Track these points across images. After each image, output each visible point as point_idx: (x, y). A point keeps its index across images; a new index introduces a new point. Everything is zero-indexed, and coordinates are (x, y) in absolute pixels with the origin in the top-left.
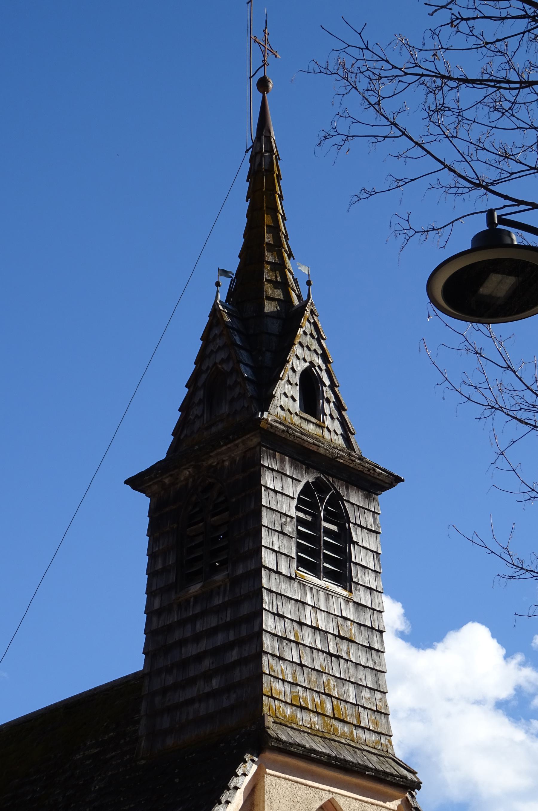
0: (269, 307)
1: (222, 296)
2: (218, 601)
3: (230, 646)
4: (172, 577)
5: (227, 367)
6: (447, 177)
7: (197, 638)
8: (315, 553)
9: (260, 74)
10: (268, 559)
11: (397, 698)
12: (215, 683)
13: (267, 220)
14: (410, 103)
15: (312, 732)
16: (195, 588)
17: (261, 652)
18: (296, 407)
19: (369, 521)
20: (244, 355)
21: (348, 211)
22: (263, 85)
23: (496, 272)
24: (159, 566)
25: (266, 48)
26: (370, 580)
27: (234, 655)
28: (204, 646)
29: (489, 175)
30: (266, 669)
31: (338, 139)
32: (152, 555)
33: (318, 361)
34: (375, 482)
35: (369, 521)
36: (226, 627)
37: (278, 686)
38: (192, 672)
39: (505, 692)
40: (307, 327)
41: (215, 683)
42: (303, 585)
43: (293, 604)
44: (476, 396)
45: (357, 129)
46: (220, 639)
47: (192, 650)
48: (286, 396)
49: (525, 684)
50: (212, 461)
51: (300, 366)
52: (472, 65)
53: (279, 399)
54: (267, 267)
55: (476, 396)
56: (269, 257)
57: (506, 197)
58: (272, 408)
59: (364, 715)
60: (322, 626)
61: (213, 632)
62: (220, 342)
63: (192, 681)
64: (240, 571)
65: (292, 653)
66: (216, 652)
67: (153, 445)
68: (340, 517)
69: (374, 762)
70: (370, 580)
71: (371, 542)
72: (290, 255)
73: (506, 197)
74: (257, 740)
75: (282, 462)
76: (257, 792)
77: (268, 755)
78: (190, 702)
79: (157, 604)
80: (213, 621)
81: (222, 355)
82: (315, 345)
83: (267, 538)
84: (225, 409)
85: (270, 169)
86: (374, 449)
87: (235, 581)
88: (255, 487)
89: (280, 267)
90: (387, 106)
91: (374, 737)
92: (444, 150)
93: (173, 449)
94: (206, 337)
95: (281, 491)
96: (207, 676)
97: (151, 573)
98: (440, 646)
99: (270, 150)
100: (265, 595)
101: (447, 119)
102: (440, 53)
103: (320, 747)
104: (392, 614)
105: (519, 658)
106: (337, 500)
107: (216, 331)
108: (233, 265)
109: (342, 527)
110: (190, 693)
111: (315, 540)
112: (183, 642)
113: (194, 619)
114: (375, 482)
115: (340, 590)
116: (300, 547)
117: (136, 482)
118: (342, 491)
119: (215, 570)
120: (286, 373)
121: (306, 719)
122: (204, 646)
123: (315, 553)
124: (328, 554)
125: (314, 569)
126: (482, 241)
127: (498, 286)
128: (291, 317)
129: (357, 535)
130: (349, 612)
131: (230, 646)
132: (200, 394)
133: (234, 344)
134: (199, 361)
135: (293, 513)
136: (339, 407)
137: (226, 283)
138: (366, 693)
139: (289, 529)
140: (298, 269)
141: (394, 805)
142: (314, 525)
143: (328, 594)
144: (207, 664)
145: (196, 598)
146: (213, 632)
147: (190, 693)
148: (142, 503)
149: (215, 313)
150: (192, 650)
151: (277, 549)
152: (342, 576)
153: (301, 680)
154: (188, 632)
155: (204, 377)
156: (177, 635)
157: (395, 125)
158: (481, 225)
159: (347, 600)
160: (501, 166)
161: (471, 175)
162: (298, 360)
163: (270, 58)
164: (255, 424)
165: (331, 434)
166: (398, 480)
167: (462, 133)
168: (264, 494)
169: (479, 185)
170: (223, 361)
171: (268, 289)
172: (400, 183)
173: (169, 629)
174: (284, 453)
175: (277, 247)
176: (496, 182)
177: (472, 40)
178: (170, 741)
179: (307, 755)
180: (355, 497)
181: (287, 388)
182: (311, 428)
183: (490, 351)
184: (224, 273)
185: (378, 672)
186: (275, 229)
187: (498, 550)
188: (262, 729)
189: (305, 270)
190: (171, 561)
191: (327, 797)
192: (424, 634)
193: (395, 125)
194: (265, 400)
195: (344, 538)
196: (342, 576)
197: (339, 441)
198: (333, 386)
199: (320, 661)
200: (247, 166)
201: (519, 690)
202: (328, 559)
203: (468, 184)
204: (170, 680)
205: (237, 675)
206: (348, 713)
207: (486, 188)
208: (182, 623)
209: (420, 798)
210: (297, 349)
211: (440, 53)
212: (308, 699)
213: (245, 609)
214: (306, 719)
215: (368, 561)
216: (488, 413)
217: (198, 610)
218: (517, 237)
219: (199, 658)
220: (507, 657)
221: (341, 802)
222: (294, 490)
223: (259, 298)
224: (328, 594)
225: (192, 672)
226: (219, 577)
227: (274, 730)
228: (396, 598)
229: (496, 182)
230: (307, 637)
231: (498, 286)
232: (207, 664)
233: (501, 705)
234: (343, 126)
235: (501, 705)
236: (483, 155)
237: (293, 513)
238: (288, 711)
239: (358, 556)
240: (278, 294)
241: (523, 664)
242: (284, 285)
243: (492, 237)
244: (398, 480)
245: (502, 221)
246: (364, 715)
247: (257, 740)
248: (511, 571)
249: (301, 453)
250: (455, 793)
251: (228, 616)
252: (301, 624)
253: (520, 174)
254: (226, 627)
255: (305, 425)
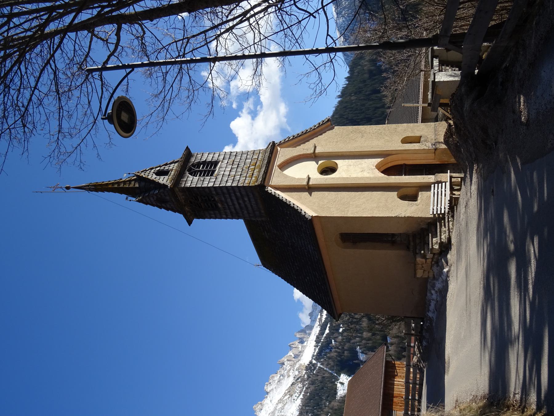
0: (137, 185)
1: (134, 199)
2: (223, 199)
3: (236, 195)
4: (217, 212)
5: (155, 197)
6: (93, 132)
7: (234, 205)
8: (209, 171)
9: (65, 189)
10: (211, 185)
11: (251, 148)
12: (246, 199)
13: (110, 186)
14: (68, 144)
15: (259, 172)
16: (220, 205)
17: (237, 186)
18: (166, 177)
19: (199, 156)
20: (152, 192)
21: (315, 147)
22: (68, 188)
23: (120, 117)
24: (213, 216)
25: (56, 187)
26: (216, 156)
27: (238, 194)
28: (236, 203)
29: (92, 120)
30: (242, 185)
31: (82, 165)
32: (210, 218)
33: (153, 171)
34: (188, 154)
35: (199, 156)
36: (230, 197)
37: (246, 181)
38: (243, 206)
39: (249, 117)
40: (142, 174)
41: (246, 199)
42: (218, 175)
43: (224, 177)
44: (160, 124)
45: (78, 159)
46: (234, 198)
47: (237, 206)
48: (163, 180)
49: (248, 111)
50: (183, 201)
51: (154, 176)
52: (54, 124)
53: (164, 182)
54: (125, 186)
55: (160, 124)
56: (122, 185)
57: (98, 114)
58: (167, 184)
59: (254, 157)
60: (229, 169)
61: (232, 200)
62: (148, 200)
63: (246, 206)
64: (214, 192)
65: (238, 177)
66: (237, 199)
67: (179, 218)
68: (199, 164)
69: (267, 154)
70: (216, 156)
71: (206, 155)
72: (121, 179)
73: (98, 114)
74: (262, 187)
75: (183, 181)
76: (277, 187)
77: (266, 184)
78: (251, 206)
79: (224, 216)
80: (229, 200)
81: (152, 199)
82: (148, 172)
83: (205, 185)
84: (168, 198)
85: (95, 185)
86: (179, 155)
87: (217, 194)
88: (190, 189)
89: (125, 182)
90: (70, 149)
91: (260, 154)
92: (84, 133)
93: (180, 213)
94: (147, 204)
95: (191, 181)
96: (244, 201)
97: (216, 218)
98: (237, 136)
99: (89, 185)
100: (221, 185)
101: (74, 132)
102: (52, 133)
103: (263, 169)
104: (228, 149)
105: (240, 113)
106: (193, 165)
107: (144, 201)
108: (124, 196)
109: (201, 164)
110: (249, 206)
111: (205, 171)
112: (235, 209)
113: (228, 205)
114: (188, 154)
115: (219, 164)
116: (204, 175)
117: (190, 223)
118: (191, 164)
119: (214, 200)
120: (157, 180)
121: (256, 174)
122: (236, 203)
123: (209, 171)
124: (209, 168)
125: (213, 172)
126: (111, 121)
127: (125, 117)
128: (140, 179)
129: (204, 159)
130: (226, 161)
131: (236, 195)
132: (163, 205)
133: (148, 195)
134: (153, 205)
135: (198, 177)
136: (166, 164)
137: (130, 198)
138: (248, 157)
139: (202, 179)
140: (125, 177)
141: (279, 149)
142: (201, 172)
143: (220, 167)
144: (241, 202)
145: (222, 205)
146: (232, 200)
147: (249, 206)
148: (195, 221)
149: (139, 201)
150: (237, 206)
151: (208, 182)
152: (216, 163)
153: (245, 175)
154: (232, 207)
155: (158, 204)
156: (233, 210)
157: (76, 148)
158: (106, 122)
159: (222, 162)
160: (88, 116)
161: (92, 125)
162: (152, 176)
163: (59, 186)
164: (172, 189)
165: (174, 167)
166: (187, 147)
167: (78, 127)
168: (192, 186)
169: (95, 122)
170: (153, 199)
171: (131, 186)
172: (95, 146)
173: (231, 212)
174: (180, 181)
175: (118, 183)
176: (94, 117)
177: (46, 123)
178: (263, 212)
179: (266, 173)
180: (193, 160)
181: (161, 180)
182: (173, 173)
183: (146, 120)
184: (127, 199)
185: (242, 153)
186: (113, 184)
187: (206, 118)
188: (258, 186)
189: (125, 175)
190: (212, 212)
191: (277, 167)
192: (234, 140)
193: (76, 148)
194: (165, 186)
195: (204, 163)
196: (216, 163)
197: (176, 164)
198: (160, 166)
199: (240, 170)
200: (94, 192)
201: (249, 113)
202: (211, 168)
203: (95, 126)
204: (246, 212)
205: (244, 193)
206: (254, 162)
207: (96, 120)
208: (229, 209)
209: (277, 141)
210: (149, 177)
211: (52, 133)
212: (250, 173)
213: (225, 191)
214: (256, 174)
215: (211, 156)
216: (165, 121)
217: (226, 204)
218: (109, 111)
219: (239, 204)
220: (240, 117)
221: (278, 163)
222: (191, 177)
223: (134, 188)
224: (220, 167)
225: (243, 206)
226: (216, 199)
227: (259, 182)
228: (223, 148)
229: (94, 117)
230: (233, 173)
231: (125, 117)
232: (241, 202)
233: (253, 118)
234: (77, 163)
235: (253, 118)
236: (85, 121)
237: (198, 177)
238: (253, 178)
239: (209, 159)
240: (133, 183)
241: (242, 112)
242: (130, 181)
243: (110, 118)
244: (187, 147)
245: (105, 115)
246: (254, 157)
247: (262, 187)
248: (211, 115)
249: (180, 175)
250: (278, 132)
251: (227, 196)
252: (229, 175)
253: (91, 110)
254: (230, 197)
255: (172, 174)
